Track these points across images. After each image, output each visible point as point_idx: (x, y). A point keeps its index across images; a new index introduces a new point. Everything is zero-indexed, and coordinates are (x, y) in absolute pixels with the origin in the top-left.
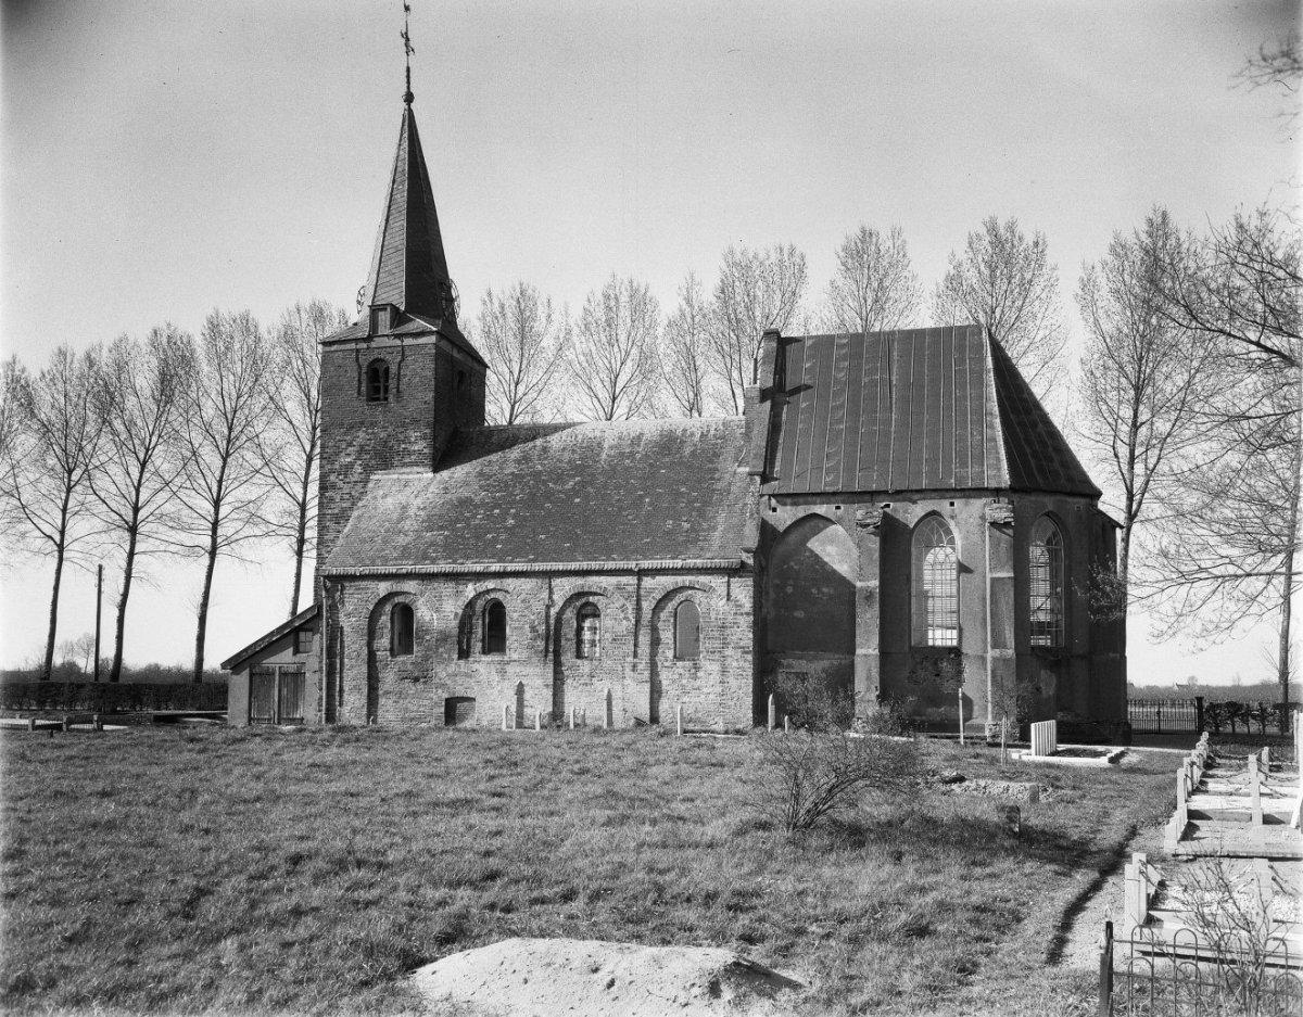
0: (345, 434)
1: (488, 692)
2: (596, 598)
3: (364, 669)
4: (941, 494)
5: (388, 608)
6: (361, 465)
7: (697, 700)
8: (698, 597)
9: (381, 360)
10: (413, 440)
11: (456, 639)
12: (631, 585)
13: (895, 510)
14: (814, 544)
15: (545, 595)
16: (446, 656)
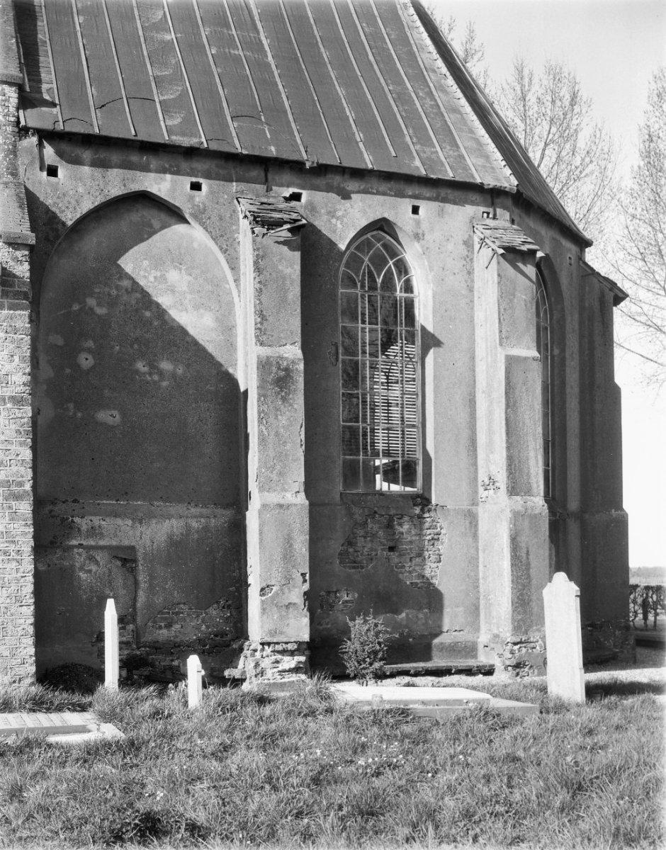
4: (401, 186)
13: (312, 207)
14: (135, 263)
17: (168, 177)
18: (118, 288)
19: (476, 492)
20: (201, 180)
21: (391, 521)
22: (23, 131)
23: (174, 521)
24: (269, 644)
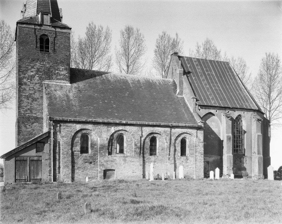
0: (30, 63)
1: (120, 167)
2: (157, 135)
3: (70, 158)
5: (79, 135)
6: (38, 77)
7: (187, 169)
8: (188, 136)
9: (46, 35)
10: (61, 69)
11: (107, 148)
12: (168, 131)
15: (140, 133)
16: (103, 154)
17: (213, 110)
18: (206, 125)
19: (252, 154)
20: (217, 110)
21: (240, 158)
22: (196, 104)
23: (214, 158)
24: (228, 175)
